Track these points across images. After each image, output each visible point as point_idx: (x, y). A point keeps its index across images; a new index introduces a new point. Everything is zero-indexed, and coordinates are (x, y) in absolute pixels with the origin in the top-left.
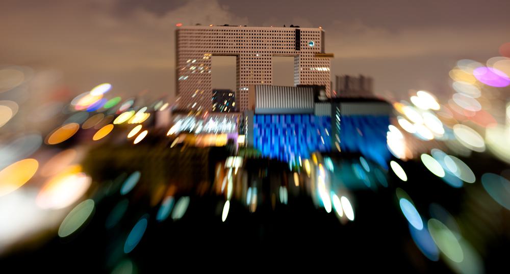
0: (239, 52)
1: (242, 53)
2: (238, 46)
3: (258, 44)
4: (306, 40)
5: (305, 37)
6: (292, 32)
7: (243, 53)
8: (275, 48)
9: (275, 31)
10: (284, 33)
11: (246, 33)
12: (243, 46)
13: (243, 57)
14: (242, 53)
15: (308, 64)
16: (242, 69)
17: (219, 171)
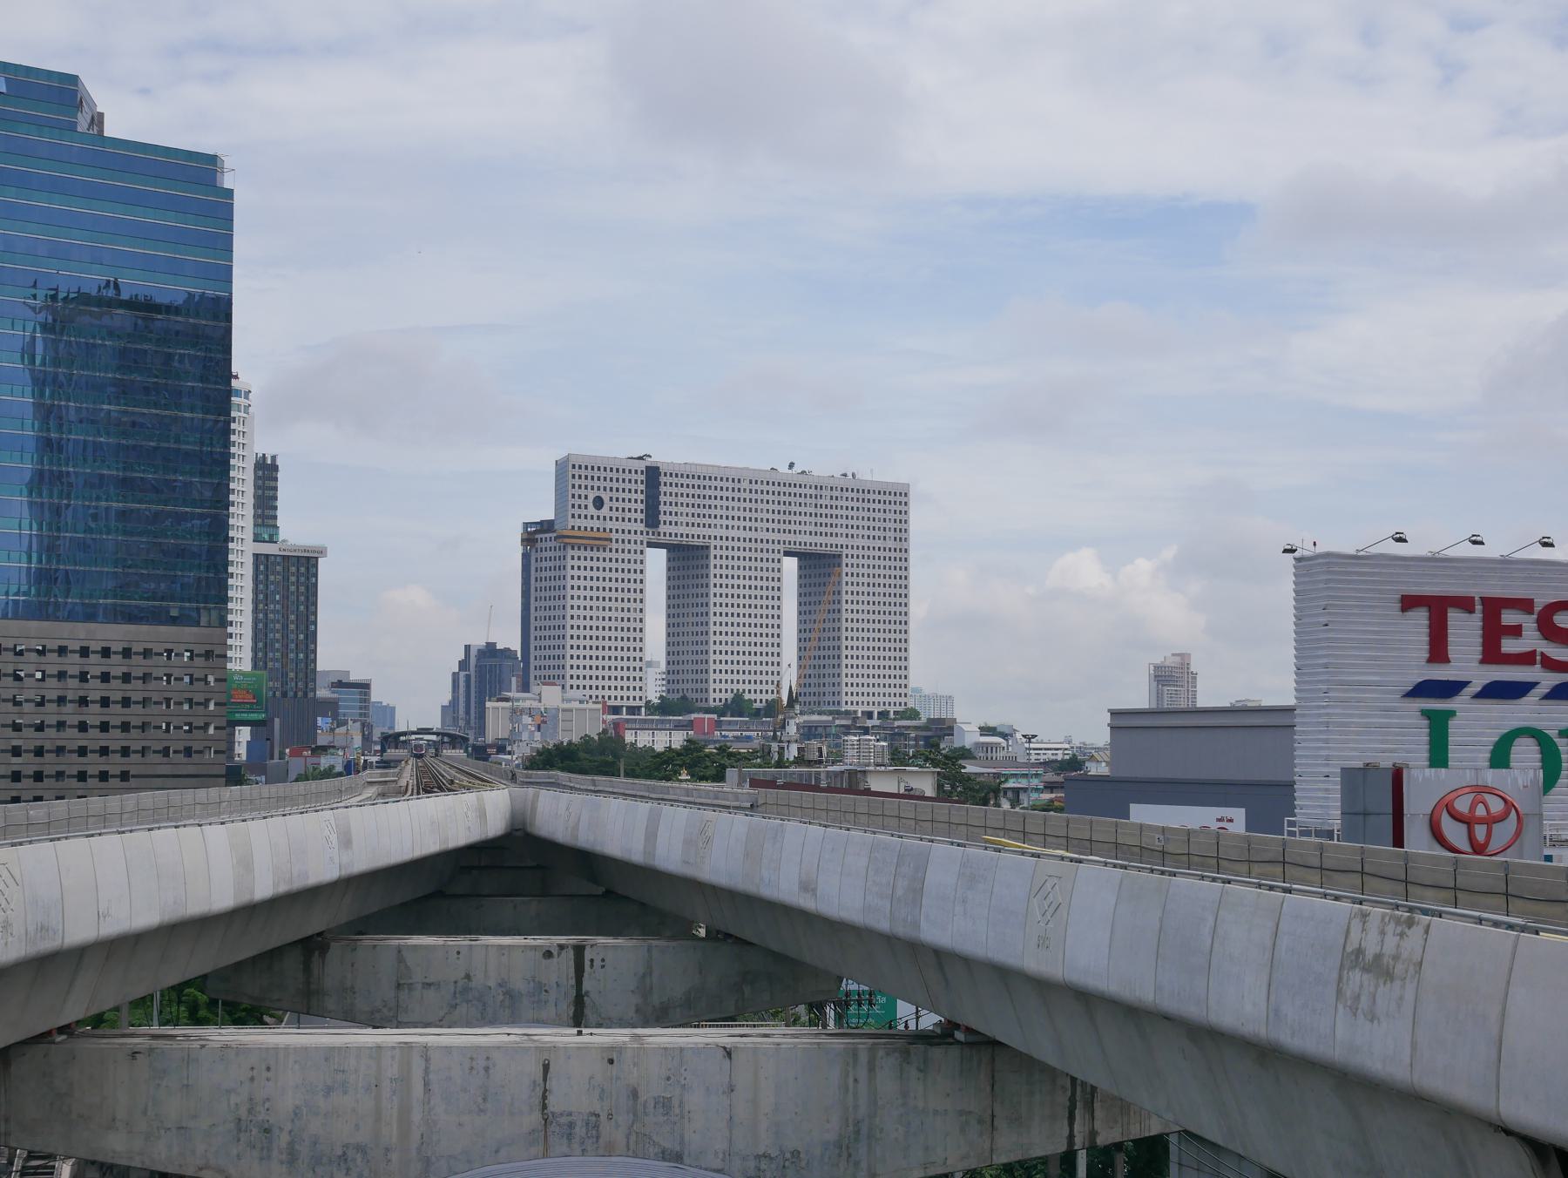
7: (850, 551)
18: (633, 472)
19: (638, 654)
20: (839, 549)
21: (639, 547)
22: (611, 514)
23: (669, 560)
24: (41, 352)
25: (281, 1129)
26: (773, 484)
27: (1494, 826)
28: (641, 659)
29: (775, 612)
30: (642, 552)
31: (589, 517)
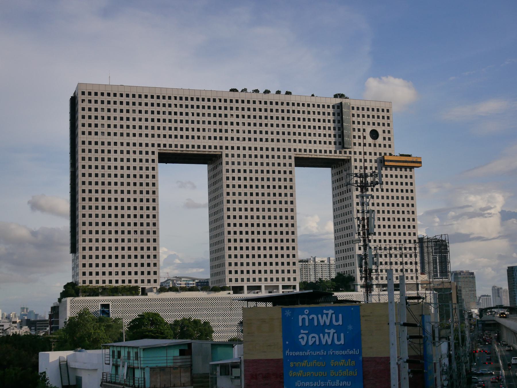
0: (221, 147)
1: (227, 152)
2: (218, 134)
3: (193, 129)
7: (230, 152)
8: (385, 146)
10: (316, 110)
11: (234, 105)
12: (229, 135)
13: (230, 159)
14: (227, 152)
16: (228, 194)
17: (79, 349)
18: (326, 107)
19: (291, 252)
20: (218, 149)
21: (150, 165)
23: (333, 175)
26: (383, 110)
28: (294, 256)
29: (410, 202)
30: (291, 172)
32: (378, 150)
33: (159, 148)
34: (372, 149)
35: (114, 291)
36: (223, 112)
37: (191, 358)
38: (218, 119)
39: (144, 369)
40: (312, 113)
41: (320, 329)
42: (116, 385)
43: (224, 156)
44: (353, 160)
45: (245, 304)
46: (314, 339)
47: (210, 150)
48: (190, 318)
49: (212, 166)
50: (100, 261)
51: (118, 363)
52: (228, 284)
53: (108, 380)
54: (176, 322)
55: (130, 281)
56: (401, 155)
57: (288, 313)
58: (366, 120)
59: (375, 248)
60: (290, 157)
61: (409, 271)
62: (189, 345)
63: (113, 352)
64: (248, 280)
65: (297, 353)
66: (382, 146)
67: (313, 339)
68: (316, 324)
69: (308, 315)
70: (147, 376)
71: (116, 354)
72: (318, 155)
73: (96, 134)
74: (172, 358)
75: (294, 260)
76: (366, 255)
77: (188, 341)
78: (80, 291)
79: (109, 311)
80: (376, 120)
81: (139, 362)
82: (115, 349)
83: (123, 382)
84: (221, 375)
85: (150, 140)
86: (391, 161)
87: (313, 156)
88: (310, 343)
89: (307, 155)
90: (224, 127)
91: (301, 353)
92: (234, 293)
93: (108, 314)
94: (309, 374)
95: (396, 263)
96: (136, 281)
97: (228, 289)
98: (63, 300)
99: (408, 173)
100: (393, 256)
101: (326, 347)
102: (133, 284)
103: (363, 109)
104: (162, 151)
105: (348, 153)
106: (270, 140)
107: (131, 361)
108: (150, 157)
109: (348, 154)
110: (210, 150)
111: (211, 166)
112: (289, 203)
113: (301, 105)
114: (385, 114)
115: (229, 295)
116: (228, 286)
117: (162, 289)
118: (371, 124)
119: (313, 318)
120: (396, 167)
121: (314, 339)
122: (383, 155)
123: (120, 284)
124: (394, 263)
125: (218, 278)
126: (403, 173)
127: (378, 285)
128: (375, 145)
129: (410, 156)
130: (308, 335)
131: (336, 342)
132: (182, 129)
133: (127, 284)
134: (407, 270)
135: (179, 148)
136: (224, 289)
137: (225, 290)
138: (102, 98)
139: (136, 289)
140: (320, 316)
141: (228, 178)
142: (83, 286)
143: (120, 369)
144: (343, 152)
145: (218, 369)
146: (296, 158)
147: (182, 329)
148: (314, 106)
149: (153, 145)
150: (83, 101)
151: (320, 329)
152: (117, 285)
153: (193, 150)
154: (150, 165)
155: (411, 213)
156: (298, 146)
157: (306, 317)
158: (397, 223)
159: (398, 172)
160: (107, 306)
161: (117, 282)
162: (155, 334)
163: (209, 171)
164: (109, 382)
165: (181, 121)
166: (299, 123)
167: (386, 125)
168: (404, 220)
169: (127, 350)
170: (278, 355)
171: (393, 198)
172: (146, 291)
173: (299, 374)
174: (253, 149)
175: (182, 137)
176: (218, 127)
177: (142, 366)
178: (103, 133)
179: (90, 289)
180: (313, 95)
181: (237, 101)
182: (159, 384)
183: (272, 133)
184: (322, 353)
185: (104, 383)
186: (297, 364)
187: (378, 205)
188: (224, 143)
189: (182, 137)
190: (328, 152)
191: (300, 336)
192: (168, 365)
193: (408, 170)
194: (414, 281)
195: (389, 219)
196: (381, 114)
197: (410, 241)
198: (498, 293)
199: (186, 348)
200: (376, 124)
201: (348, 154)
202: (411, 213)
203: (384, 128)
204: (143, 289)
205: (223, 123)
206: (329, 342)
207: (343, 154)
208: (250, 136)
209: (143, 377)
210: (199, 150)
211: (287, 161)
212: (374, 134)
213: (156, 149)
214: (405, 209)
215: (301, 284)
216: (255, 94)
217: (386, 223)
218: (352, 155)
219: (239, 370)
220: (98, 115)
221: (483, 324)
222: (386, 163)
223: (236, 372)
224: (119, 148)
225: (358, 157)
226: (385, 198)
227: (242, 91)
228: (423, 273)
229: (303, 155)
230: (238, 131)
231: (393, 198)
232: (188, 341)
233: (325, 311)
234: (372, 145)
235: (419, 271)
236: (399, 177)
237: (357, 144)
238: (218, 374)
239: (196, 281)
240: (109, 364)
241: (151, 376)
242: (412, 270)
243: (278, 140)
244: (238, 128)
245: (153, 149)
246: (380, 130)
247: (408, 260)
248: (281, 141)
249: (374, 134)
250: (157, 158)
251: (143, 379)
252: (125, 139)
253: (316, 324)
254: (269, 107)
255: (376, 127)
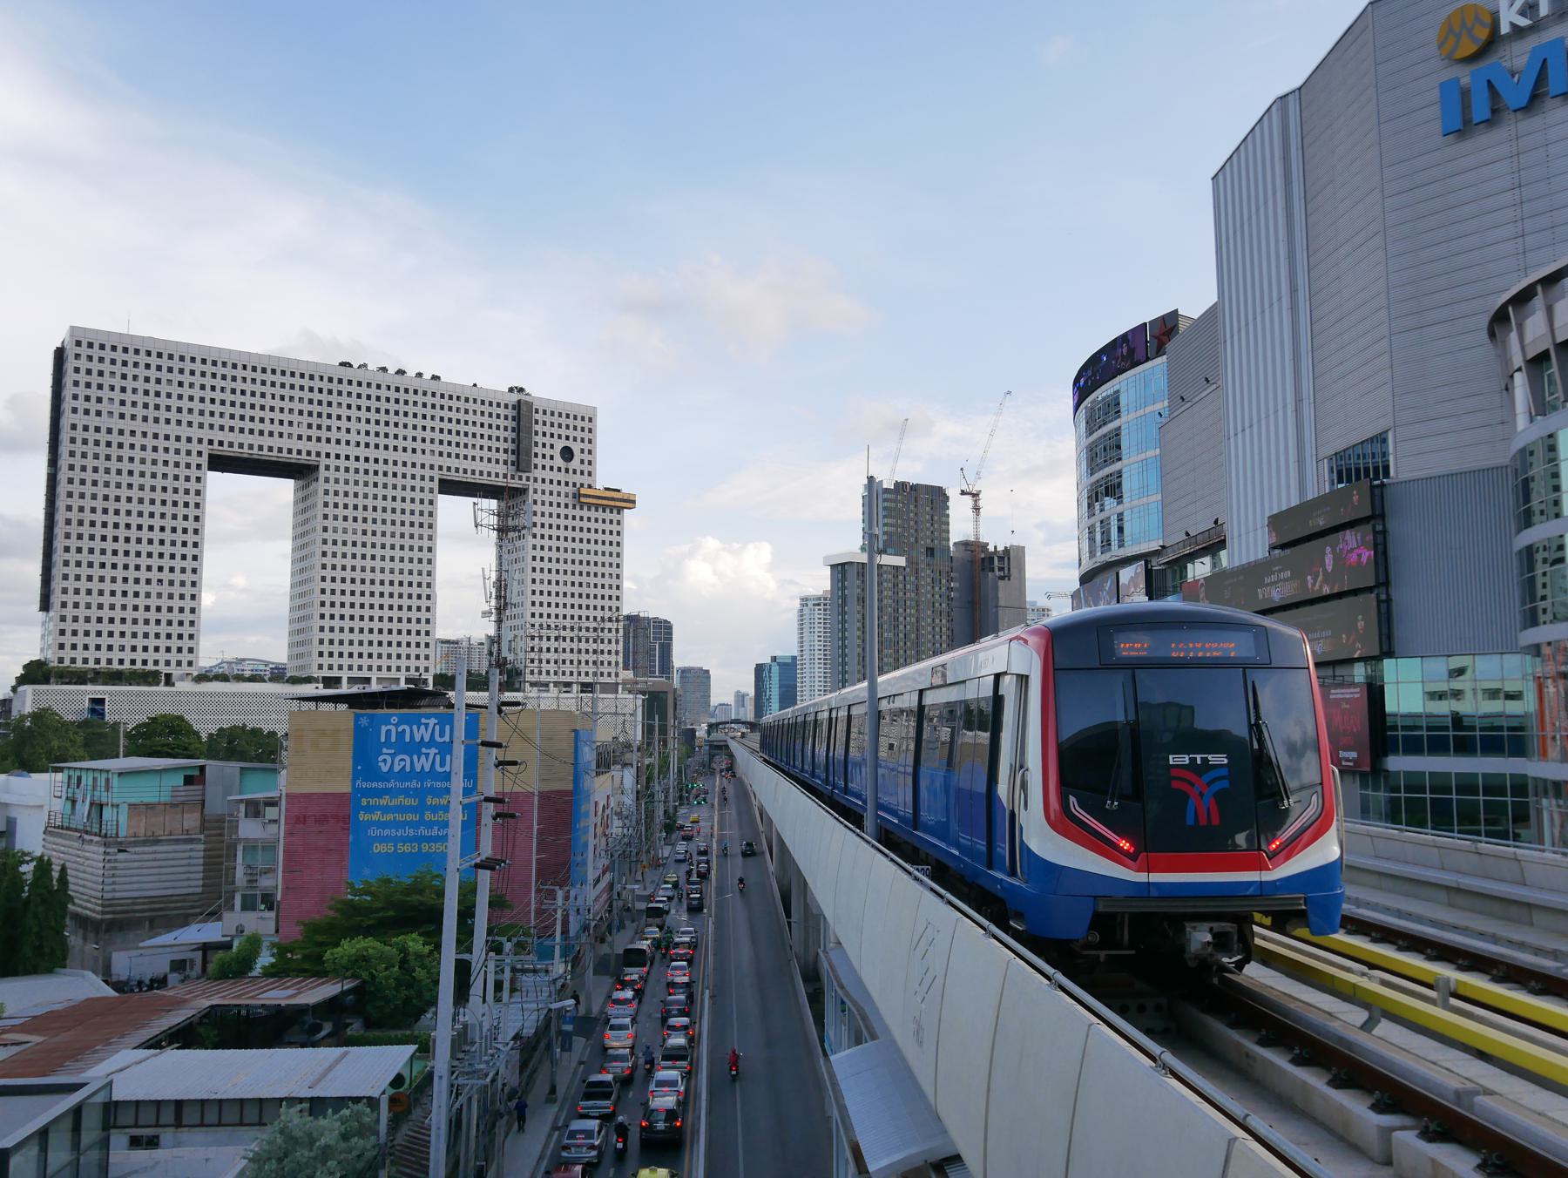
0: (318, 454)
1: (327, 461)
4: (552, 441)
5: (547, 429)
6: (506, 406)
8: (582, 473)
9: (451, 397)
10: (479, 408)
14: (327, 461)
15: (97, 558)
20: (313, 457)
22: (582, 467)
24: (483, 829)
25: (1108, 593)
26: (583, 419)
27: (1370, 513)
30: (431, 502)
31: (555, 469)
32: (571, 478)
33: (210, 447)
34: (562, 477)
35: (115, 677)
36: (324, 397)
37: (204, 790)
38: (316, 408)
39: (117, 806)
40: (471, 412)
41: (414, 748)
42: (69, 832)
43: (322, 468)
44: (531, 491)
45: (295, 705)
46: (402, 763)
47: (299, 457)
48: (245, 725)
49: (301, 483)
50: (404, 638)
51: (76, 796)
52: (317, 674)
53: (57, 824)
54: (221, 729)
55: (145, 662)
56: (606, 489)
57: (364, 722)
58: (555, 430)
59: (557, 626)
60: (432, 479)
61: (606, 663)
62: (202, 768)
63: (69, 777)
64: (350, 667)
65: (374, 785)
66: (578, 472)
67: (401, 762)
68: (408, 739)
69: (397, 725)
70: (123, 819)
71: (74, 781)
72: (477, 479)
73: (99, 413)
74: (170, 789)
75: (427, 639)
76: (499, 636)
77: (201, 762)
78: (53, 674)
79: (103, 710)
80: (571, 433)
81: (110, 794)
82: (72, 773)
83: (82, 828)
84: (246, 816)
85: (428, 459)
86: (589, 496)
87: (469, 480)
88: (397, 768)
89: (460, 477)
90: (325, 422)
91: (381, 785)
92: (325, 688)
93: (102, 714)
94: (389, 817)
95: (587, 651)
96: (156, 663)
97: (316, 680)
98: (21, 689)
99: (615, 517)
100: (583, 640)
101: (422, 775)
102: (150, 667)
103: (442, 396)
104: (214, 452)
105: (524, 479)
106: (400, 449)
107: (97, 794)
108: (427, 484)
109: (524, 481)
110: (299, 457)
111: (300, 482)
112: (425, 549)
113: (455, 398)
114: (586, 424)
115: (316, 691)
116: (316, 675)
117: (202, 678)
118: (564, 437)
119: (404, 730)
120: (597, 507)
121: (402, 763)
122: (578, 486)
123: (127, 665)
124: (583, 651)
125: (299, 662)
126: (608, 516)
127: (533, 684)
128: (567, 471)
129: (619, 491)
130: (393, 756)
131: (438, 768)
132: (252, 419)
133: (139, 665)
134: (602, 663)
135: (275, 453)
136: (309, 680)
137: (310, 682)
138: (359, 390)
139: (156, 674)
140: (415, 727)
141: (326, 505)
142: (58, 667)
143: (78, 805)
144: (517, 478)
145: (242, 807)
146: (441, 481)
147: (230, 742)
148: (475, 401)
149: (200, 441)
150: (77, 356)
151: (414, 748)
152: (121, 667)
153: (270, 454)
154: (427, 496)
155: (614, 576)
156: (446, 462)
157: (393, 729)
158: (592, 591)
159: (600, 515)
160: (102, 701)
161: (121, 662)
162: (173, 749)
163: (296, 491)
164: (59, 827)
165: (253, 406)
166: (450, 426)
167: (586, 441)
168: (603, 586)
169: (91, 774)
170: (343, 786)
171: (589, 552)
172: (173, 680)
173: (375, 817)
174: (372, 460)
175: (466, 457)
176: (315, 421)
177: (115, 801)
178: (110, 413)
179: (72, 672)
180: (475, 385)
181: (416, 392)
182: (143, 831)
183: (405, 438)
184: (414, 784)
185: (49, 829)
186: (372, 802)
187: (566, 562)
188: (324, 448)
189: (449, 455)
190: (493, 475)
191: (380, 759)
192: (163, 800)
193: (615, 511)
194: (612, 680)
195: (557, 583)
196: (579, 424)
197: (595, 618)
198: (743, 701)
199: (196, 773)
200: (571, 439)
201: (524, 481)
202: (614, 576)
203: (582, 446)
204: (168, 676)
205: (324, 416)
206: (427, 769)
207: (517, 480)
208: (367, 439)
209: (115, 818)
210: (280, 455)
211: (562, 500)
212: (567, 454)
213: (436, 474)
214: (607, 570)
215: (435, 677)
216: (399, 377)
217: (576, 590)
218: (531, 482)
219: (277, 809)
220: (104, 383)
221: (710, 746)
222: (582, 499)
223: (271, 813)
224: (381, 467)
225: (539, 486)
226: (585, 552)
227: (359, 367)
228: (626, 667)
229: (453, 476)
230: (348, 431)
231: (581, 552)
232: (201, 762)
233: (423, 720)
234: (563, 470)
235: (621, 665)
236: (600, 521)
237: (540, 467)
238: (242, 814)
239: (271, 666)
240: (60, 797)
241: (130, 817)
242: (609, 663)
243: (414, 451)
244: (348, 425)
245: (432, 473)
246: (576, 448)
247: (605, 647)
248: (276, 434)
249: (567, 454)
250: (207, 463)
251: (115, 823)
252: (151, 428)
253: (408, 739)
254: (402, 396)
255: (569, 444)
